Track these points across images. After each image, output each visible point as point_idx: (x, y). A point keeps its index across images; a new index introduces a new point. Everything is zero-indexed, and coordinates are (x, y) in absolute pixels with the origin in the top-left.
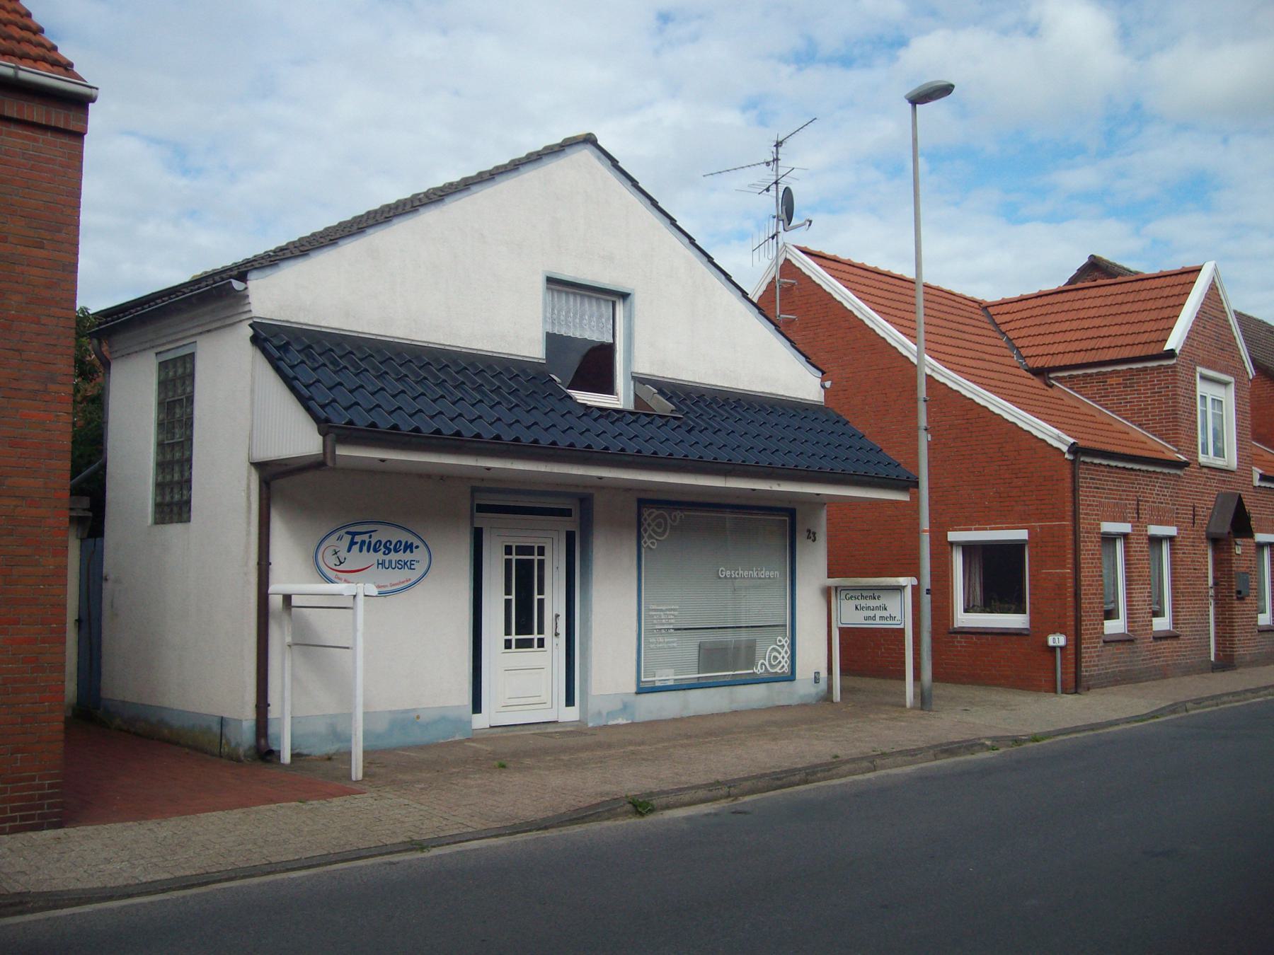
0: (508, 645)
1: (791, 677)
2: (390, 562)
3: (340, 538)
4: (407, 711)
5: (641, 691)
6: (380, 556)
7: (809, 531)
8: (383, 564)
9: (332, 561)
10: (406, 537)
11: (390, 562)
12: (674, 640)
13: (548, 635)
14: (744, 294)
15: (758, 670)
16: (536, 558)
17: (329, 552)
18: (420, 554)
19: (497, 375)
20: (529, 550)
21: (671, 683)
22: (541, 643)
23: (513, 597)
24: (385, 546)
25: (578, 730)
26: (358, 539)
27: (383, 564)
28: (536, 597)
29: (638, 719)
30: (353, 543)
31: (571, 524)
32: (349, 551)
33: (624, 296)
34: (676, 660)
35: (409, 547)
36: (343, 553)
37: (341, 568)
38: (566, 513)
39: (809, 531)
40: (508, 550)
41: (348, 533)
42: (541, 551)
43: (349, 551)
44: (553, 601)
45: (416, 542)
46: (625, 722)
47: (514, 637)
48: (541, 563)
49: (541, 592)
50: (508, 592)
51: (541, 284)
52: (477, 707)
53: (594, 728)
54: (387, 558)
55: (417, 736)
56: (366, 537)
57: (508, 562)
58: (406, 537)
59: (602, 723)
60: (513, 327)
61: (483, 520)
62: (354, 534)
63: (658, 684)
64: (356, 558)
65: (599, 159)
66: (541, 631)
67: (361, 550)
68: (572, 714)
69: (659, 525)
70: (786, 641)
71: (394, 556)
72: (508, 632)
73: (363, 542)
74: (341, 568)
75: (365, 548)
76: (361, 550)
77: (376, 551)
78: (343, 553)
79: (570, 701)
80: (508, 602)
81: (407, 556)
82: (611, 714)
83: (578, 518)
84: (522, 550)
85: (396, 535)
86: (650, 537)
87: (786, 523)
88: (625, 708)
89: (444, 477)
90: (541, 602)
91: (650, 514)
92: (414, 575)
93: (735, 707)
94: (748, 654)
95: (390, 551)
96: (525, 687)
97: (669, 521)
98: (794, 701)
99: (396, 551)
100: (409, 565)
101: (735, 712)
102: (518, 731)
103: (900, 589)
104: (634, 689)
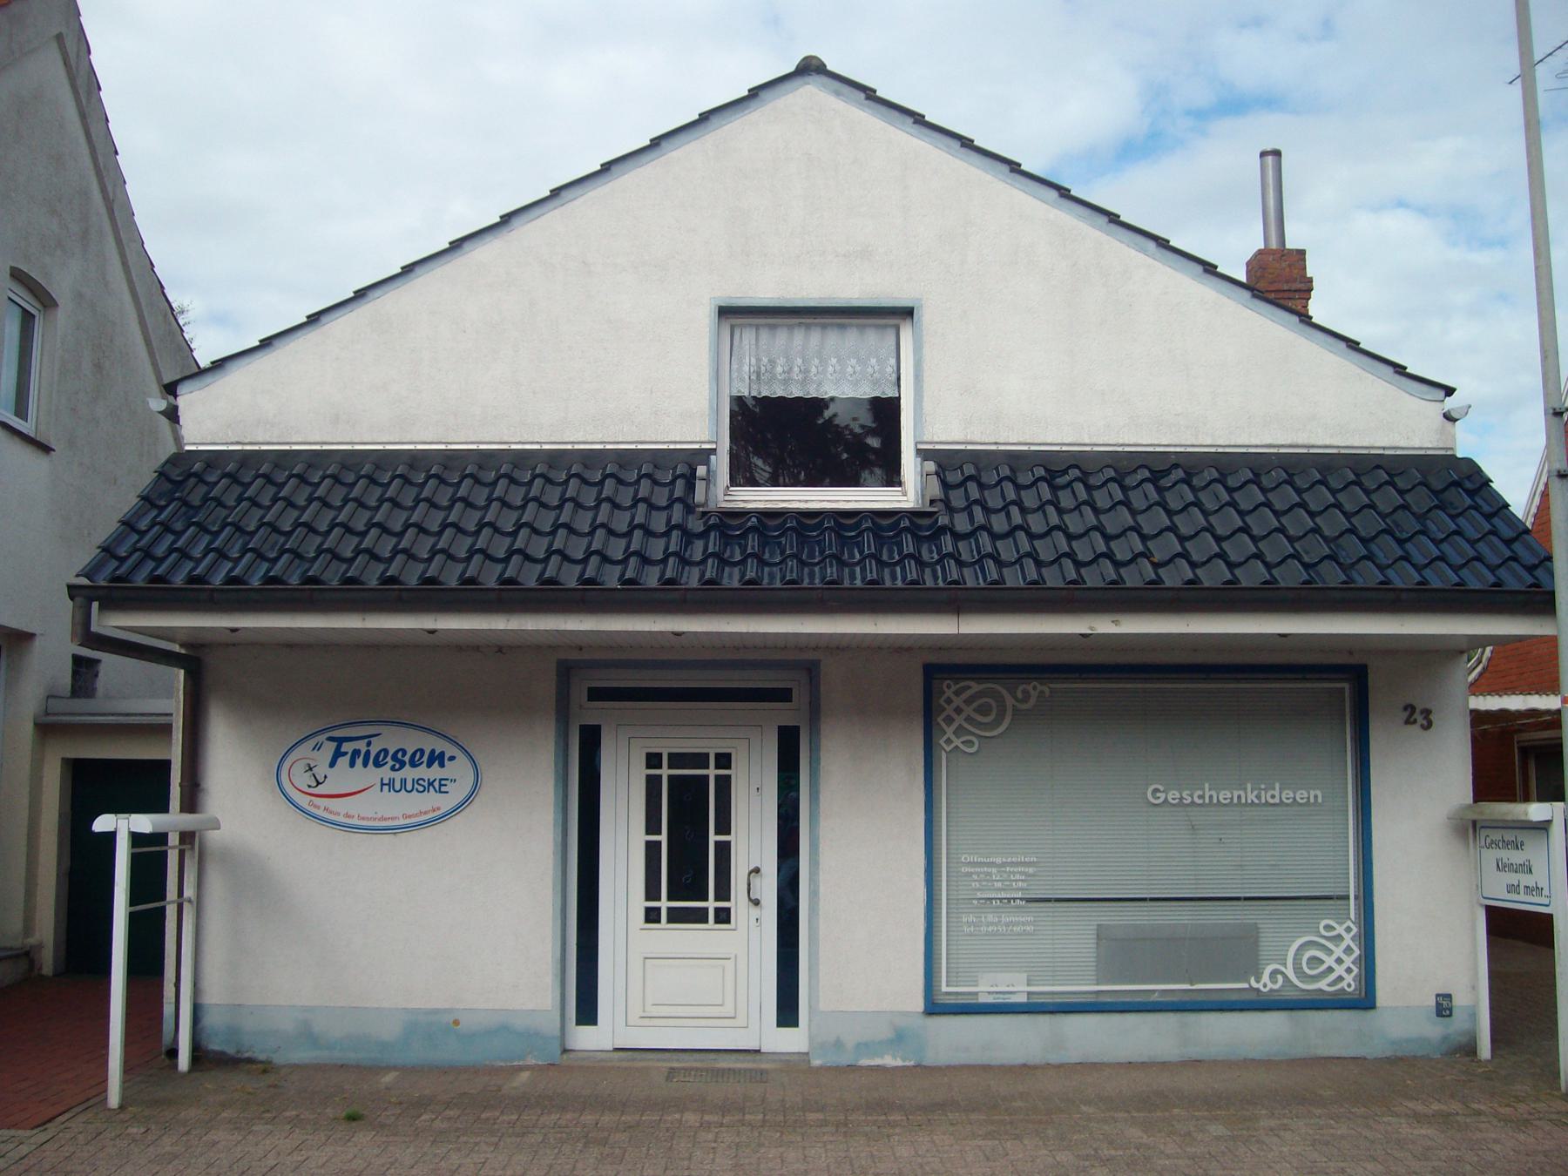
0: (652, 916)
1: (1365, 1000)
2: (403, 782)
3: (318, 747)
4: (435, 1012)
5: (935, 1008)
6: (385, 772)
7: (1410, 708)
8: (391, 784)
9: (304, 780)
10: (431, 743)
11: (403, 782)
12: (1025, 919)
13: (738, 901)
14: (1209, 269)
15: (1265, 984)
16: (712, 772)
17: (299, 769)
18: (458, 770)
19: (233, 478)
20: (700, 760)
21: (1023, 999)
22: (723, 916)
23: (663, 838)
24: (394, 757)
25: (794, 1065)
26: (348, 747)
27: (391, 784)
28: (713, 838)
29: (930, 1059)
30: (338, 754)
31: (784, 714)
32: (332, 765)
33: (908, 313)
34: (1066, 955)
35: (437, 759)
36: (322, 769)
37: (320, 790)
38: (783, 695)
39: (1410, 708)
40: (653, 760)
41: (331, 739)
42: (724, 760)
43: (332, 765)
44: (752, 842)
45: (450, 750)
46: (899, 1063)
47: (664, 904)
48: (724, 785)
49: (724, 826)
50: (652, 826)
51: (705, 317)
52: (587, 1012)
53: (821, 1068)
54: (398, 776)
55: (450, 1052)
56: (361, 745)
57: (653, 784)
58: (431, 743)
59: (844, 1060)
60: (666, 399)
61: (593, 713)
62: (340, 741)
63: (983, 999)
64: (344, 777)
65: (837, 94)
66: (723, 892)
67: (352, 764)
68: (791, 1041)
69: (984, 710)
70: (1348, 930)
71: (409, 773)
72: (652, 892)
73: (356, 753)
74: (320, 790)
75: (359, 761)
76: (352, 764)
77: (377, 764)
78: (322, 769)
79: (787, 1013)
80: (652, 850)
81: (435, 772)
82: (864, 1047)
83: (792, 703)
84: (677, 760)
85: (412, 741)
86: (959, 731)
87: (1346, 700)
88: (899, 1038)
89: (501, 648)
90: (724, 850)
91: (948, 689)
92: (446, 803)
93: (1194, 1052)
94: (1241, 951)
95: (402, 764)
96: (684, 987)
97: (1010, 701)
98: (1374, 1049)
99: (413, 764)
100: (439, 786)
101: (1195, 1063)
102: (651, 1061)
103: (1544, 827)
104: (919, 1004)
